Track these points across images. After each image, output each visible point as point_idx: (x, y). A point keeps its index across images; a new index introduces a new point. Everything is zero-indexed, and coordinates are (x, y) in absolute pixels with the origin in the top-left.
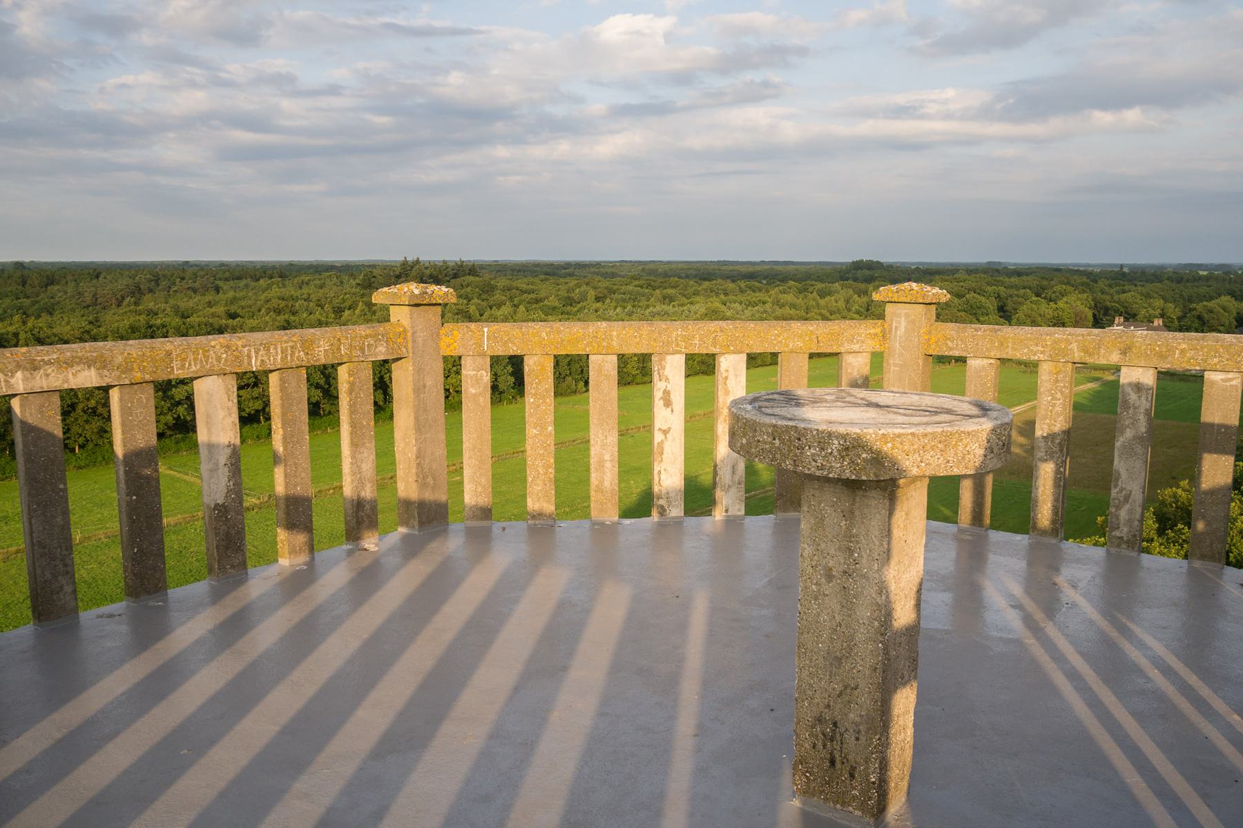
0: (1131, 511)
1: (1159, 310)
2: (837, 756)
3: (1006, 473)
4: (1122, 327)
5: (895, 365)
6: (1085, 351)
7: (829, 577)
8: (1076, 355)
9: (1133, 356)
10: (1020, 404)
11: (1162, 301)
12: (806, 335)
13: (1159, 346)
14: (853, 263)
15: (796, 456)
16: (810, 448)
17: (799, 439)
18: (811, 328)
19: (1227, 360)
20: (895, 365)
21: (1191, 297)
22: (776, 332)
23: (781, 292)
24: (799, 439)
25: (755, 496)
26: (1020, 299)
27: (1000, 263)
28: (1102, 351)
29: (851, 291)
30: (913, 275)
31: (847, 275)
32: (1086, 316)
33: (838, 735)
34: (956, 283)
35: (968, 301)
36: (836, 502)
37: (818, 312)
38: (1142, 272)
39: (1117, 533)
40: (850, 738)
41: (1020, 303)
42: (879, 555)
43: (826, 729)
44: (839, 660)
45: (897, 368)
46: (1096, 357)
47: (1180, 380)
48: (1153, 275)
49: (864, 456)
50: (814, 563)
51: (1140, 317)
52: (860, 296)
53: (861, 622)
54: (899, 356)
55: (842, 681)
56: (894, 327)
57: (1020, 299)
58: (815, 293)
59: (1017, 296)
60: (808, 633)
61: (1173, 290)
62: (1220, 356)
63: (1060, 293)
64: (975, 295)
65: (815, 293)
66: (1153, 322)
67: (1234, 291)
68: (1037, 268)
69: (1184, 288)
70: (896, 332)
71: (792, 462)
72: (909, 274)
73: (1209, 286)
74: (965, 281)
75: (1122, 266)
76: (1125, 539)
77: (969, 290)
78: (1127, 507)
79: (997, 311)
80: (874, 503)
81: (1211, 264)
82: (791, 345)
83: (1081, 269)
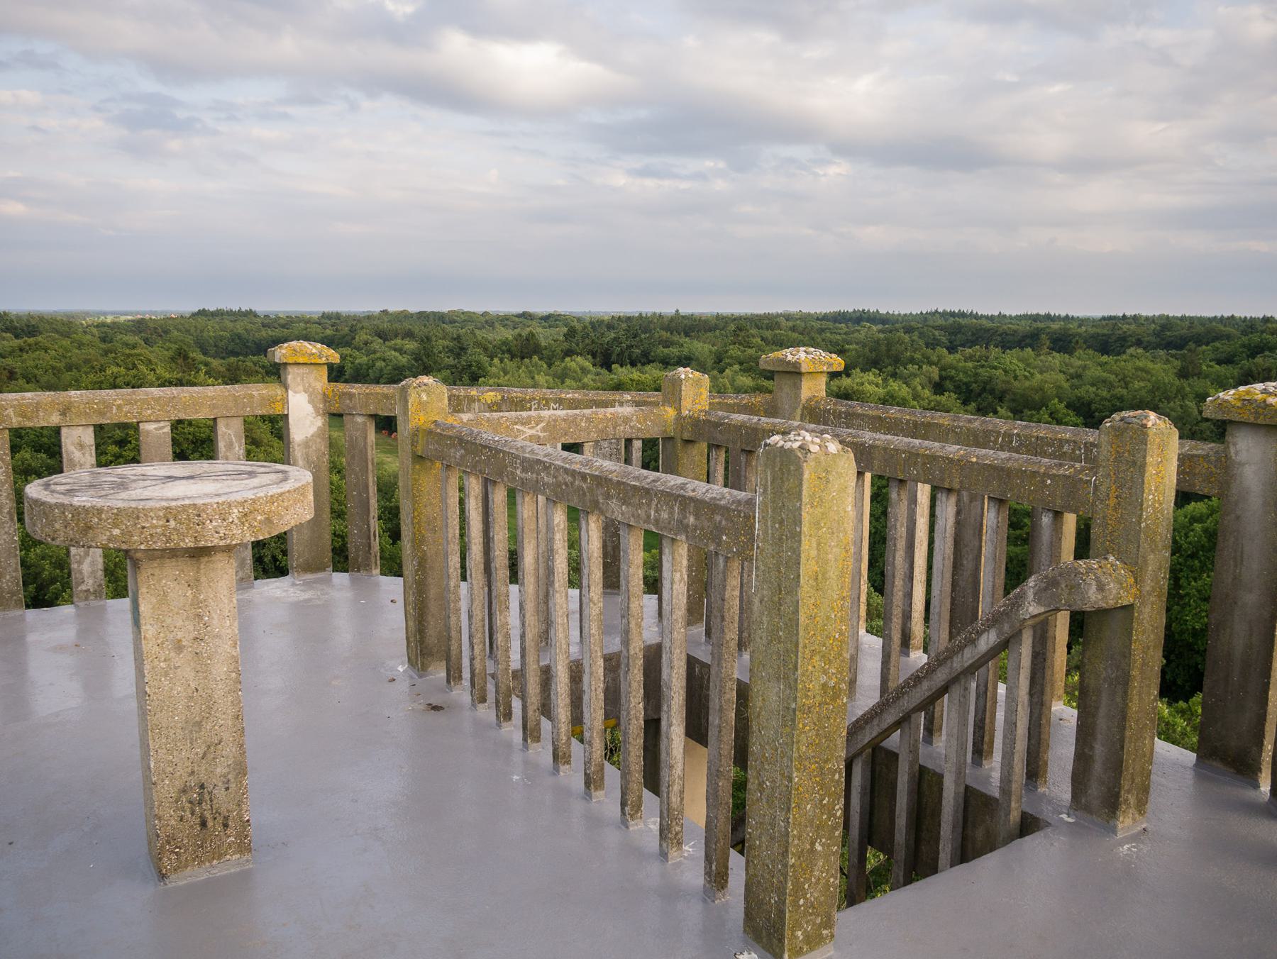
0: (93, 563)
2: (208, 816)
6: (23, 415)
7: (179, 647)
8: (14, 420)
9: (74, 416)
13: (96, 404)
15: (197, 532)
16: (211, 521)
17: (199, 516)
19: (159, 411)
24: (199, 516)
28: (41, 414)
33: (207, 797)
36: (179, 575)
39: (83, 587)
40: (220, 793)
42: (229, 611)
43: (192, 796)
44: (199, 724)
46: (36, 420)
49: (259, 518)
50: (159, 642)
53: (218, 679)
55: (205, 742)
60: (161, 711)
62: (152, 408)
71: (193, 539)
76: (91, 590)
78: (89, 560)
80: (220, 565)
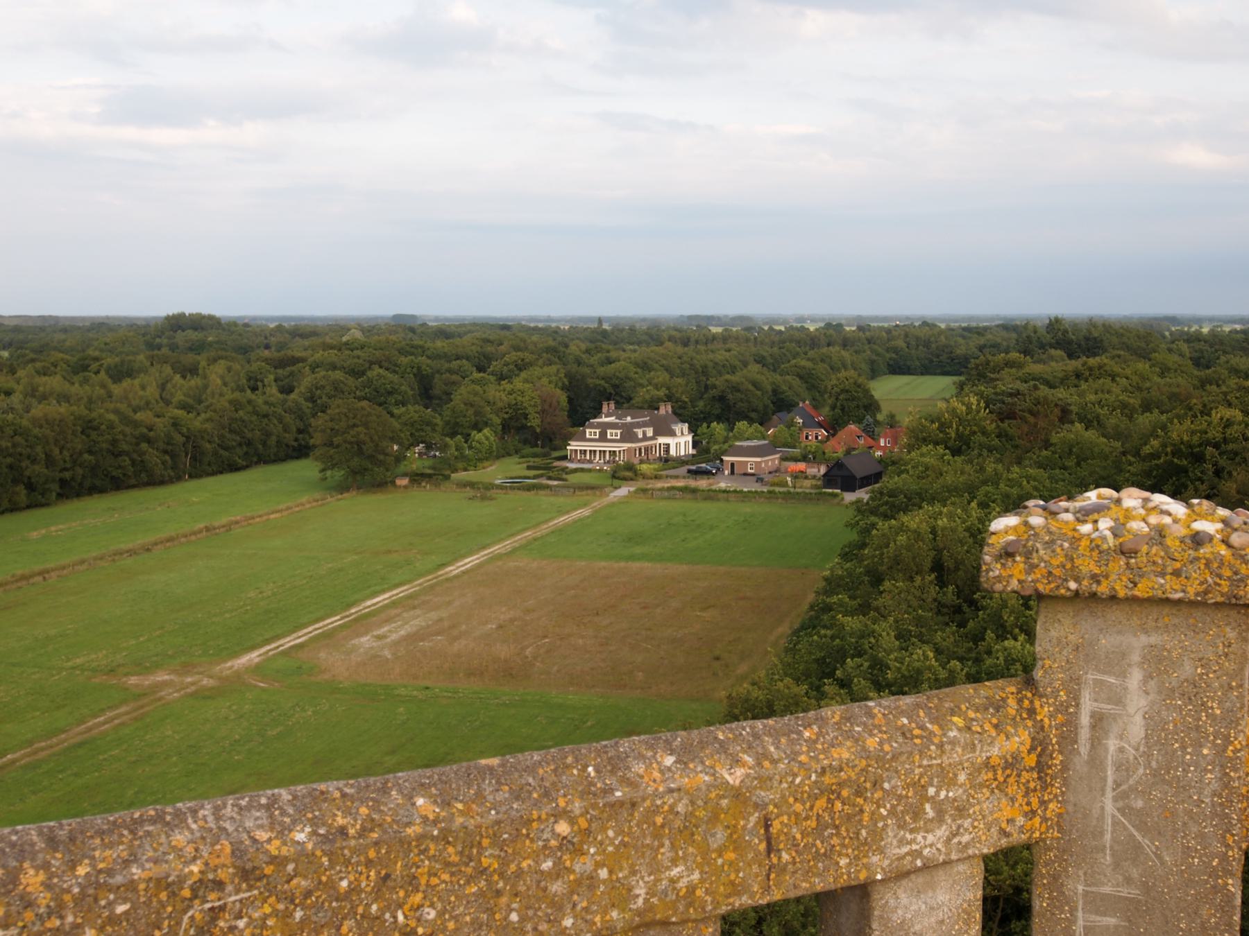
1: (664, 389)
3: (461, 675)
4: (613, 418)
5: (1097, 903)
10: (470, 553)
11: (667, 376)
12: (714, 818)
14: (168, 318)
18: (735, 777)
20: (1097, 903)
21: (706, 367)
22: (563, 828)
23: (38, 373)
25: (13, 762)
26: (455, 377)
27: (413, 317)
29: (168, 370)
30: (273, 339)
31: (158, 340)
32: (558, 402)
34: (347, 352)
35: (370, 381)
37: (112, 406)
38: (631, 329)
41: (454, 383)
45: (1112, 921)
47: (706, 499)
48: (646, 334)
51: (637, 400)
52: (184, 377)
54: (1117, 865)
56: (1085, 720)
57: (455, 377)
58: (103, 373)
59: (450, 371)
61: (680, 358)
63: (516, 366)
64: (381, 371)
65: (103, 373)
66: (658, 409)
67: (763, 357)
68: (475, 324)
69: (694, 354)
70: (1096, 742)
72: (266, 338)
73: (729, 350)
74: (362, 348)
75: (600, 321)
77: (371, 363)
79: (418, 398)
81: (726, 316)
82: (641, 891)
83: (540, 325)
